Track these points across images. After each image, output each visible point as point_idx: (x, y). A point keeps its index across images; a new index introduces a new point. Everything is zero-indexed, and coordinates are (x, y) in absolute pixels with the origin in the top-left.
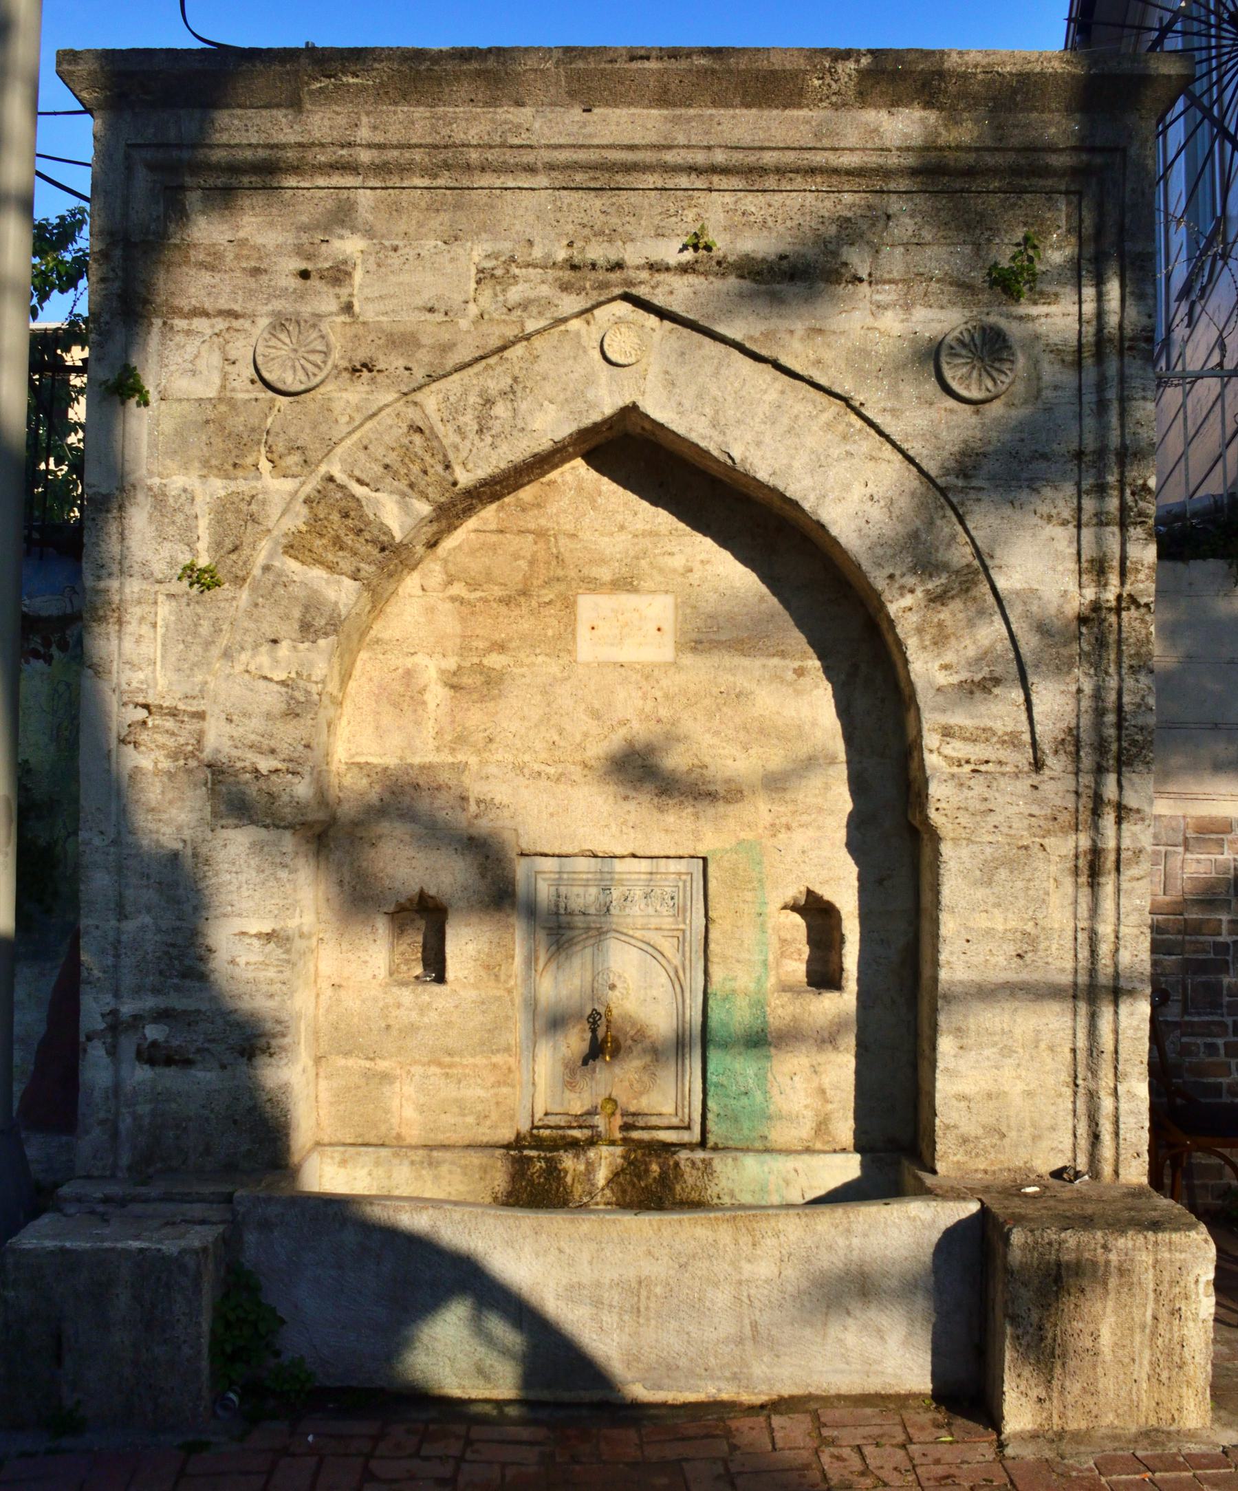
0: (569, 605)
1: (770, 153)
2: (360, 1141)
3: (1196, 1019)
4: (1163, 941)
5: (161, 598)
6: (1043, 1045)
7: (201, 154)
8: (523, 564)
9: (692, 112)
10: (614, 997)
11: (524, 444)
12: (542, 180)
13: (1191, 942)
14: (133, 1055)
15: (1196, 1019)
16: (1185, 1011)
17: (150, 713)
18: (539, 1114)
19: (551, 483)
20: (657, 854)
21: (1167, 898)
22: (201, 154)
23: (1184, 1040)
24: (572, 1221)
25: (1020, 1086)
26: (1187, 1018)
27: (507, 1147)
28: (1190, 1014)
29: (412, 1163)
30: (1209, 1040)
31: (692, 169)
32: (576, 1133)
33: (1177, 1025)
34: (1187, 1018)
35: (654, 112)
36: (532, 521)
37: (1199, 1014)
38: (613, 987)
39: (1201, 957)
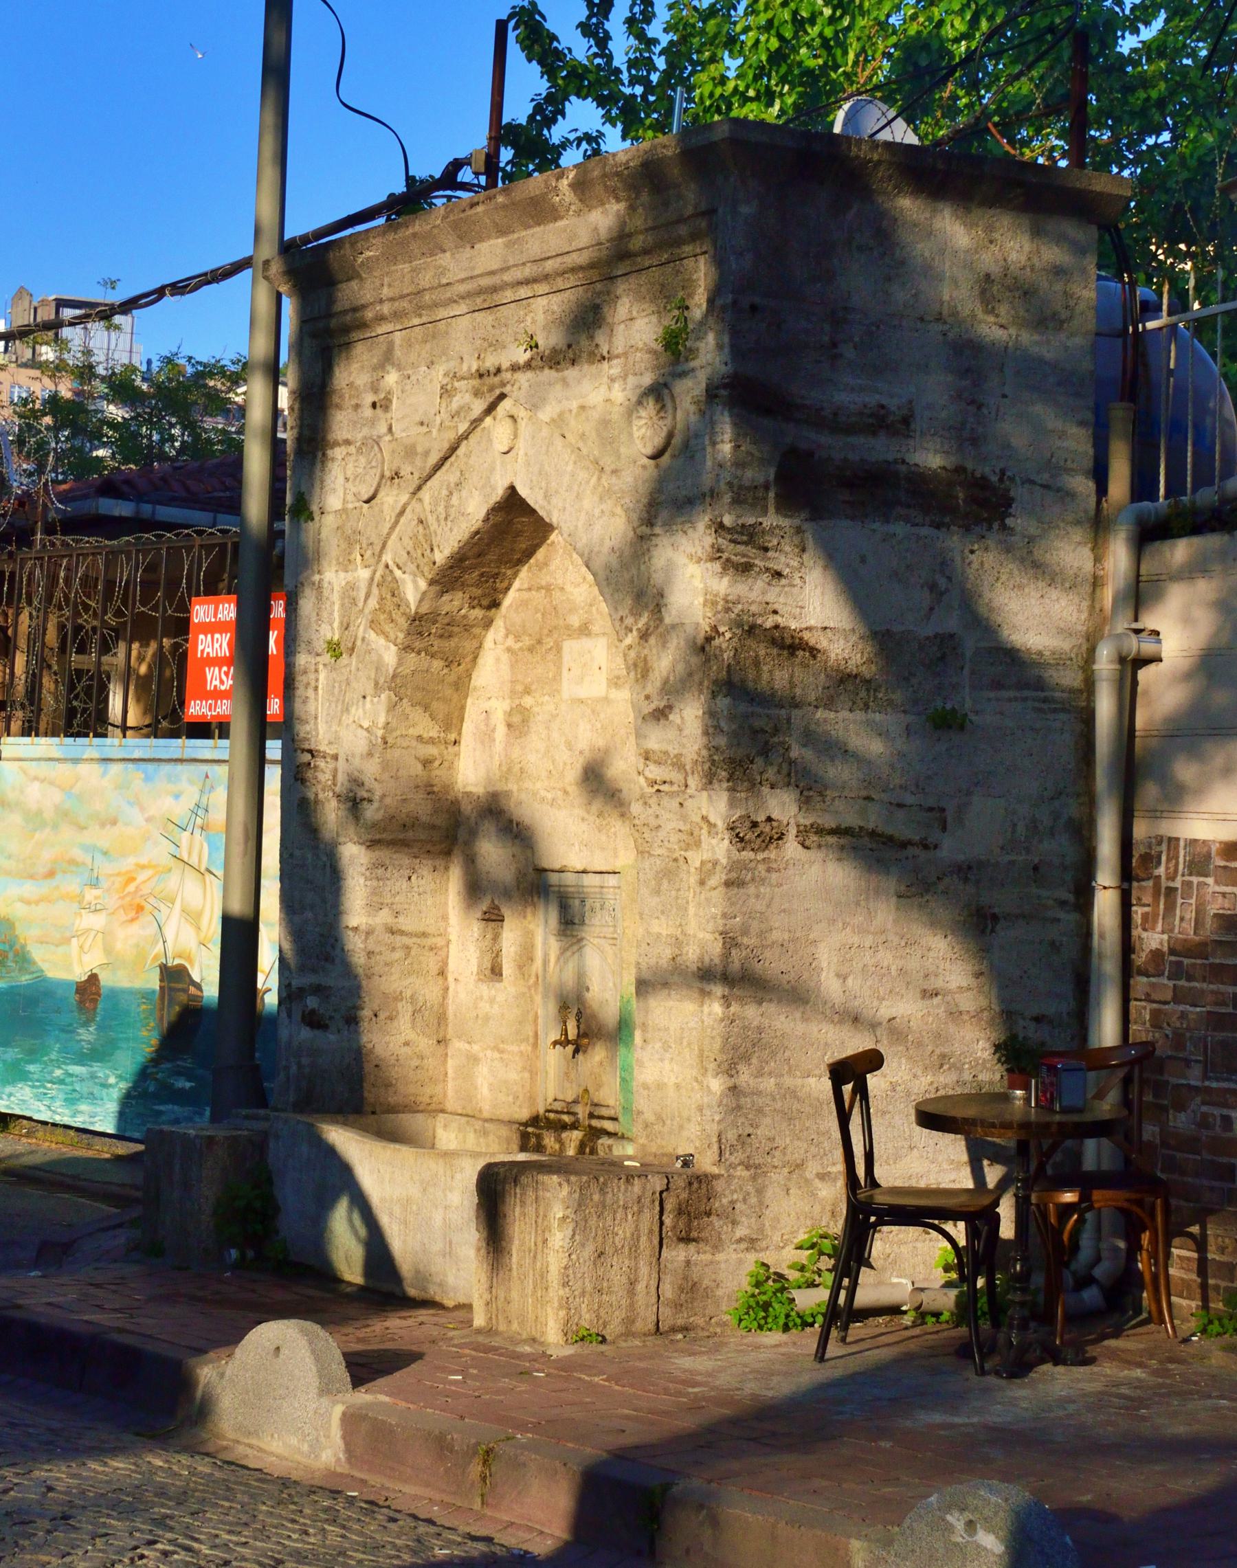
0: (558, 649)
1: (550, 262)
2: (464, 1112)
3: (1214, 1085)
4: (1191, 989)
5: (321, 667)
6: (685, 1043)
7: (334, 323)
8: (539, 615)
9: (516, 236)
10: (588, 996)
11: (464, 526)
12: (462, 308)
13: (1212, 992)
14: (299, 1018)
15: (1214, 1085)
16: (1205, 1077)
17: (313, 756)
18: (550, 1100)
19: (553, 542)
20: (604, 869)
21: (1197, 938)
22: (334, 323)
23: (1204, 1109)
24: (384, 1148)
25: (673, 1080)
26: (1207, 1083)
27: (521, 1124)
28: (1209, 1079)
29: (475, 1131)
30: (1225, 1112)
31: (527, 282)
32: (566, 1118)
33: (1196, 1089)
34: (1207, 1083)
35: (500, 240)
36: (545, 579)
37: (1217, 1080)
38: (588, 989)
39: (1223, 1010)
